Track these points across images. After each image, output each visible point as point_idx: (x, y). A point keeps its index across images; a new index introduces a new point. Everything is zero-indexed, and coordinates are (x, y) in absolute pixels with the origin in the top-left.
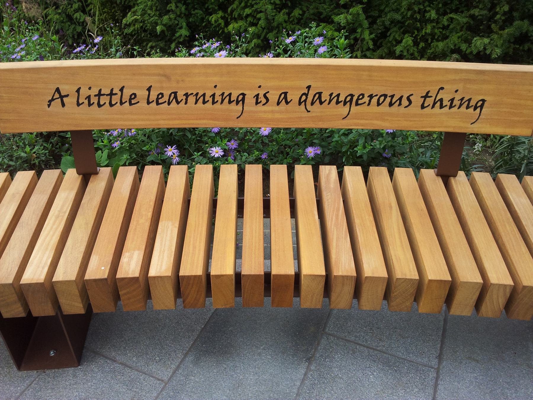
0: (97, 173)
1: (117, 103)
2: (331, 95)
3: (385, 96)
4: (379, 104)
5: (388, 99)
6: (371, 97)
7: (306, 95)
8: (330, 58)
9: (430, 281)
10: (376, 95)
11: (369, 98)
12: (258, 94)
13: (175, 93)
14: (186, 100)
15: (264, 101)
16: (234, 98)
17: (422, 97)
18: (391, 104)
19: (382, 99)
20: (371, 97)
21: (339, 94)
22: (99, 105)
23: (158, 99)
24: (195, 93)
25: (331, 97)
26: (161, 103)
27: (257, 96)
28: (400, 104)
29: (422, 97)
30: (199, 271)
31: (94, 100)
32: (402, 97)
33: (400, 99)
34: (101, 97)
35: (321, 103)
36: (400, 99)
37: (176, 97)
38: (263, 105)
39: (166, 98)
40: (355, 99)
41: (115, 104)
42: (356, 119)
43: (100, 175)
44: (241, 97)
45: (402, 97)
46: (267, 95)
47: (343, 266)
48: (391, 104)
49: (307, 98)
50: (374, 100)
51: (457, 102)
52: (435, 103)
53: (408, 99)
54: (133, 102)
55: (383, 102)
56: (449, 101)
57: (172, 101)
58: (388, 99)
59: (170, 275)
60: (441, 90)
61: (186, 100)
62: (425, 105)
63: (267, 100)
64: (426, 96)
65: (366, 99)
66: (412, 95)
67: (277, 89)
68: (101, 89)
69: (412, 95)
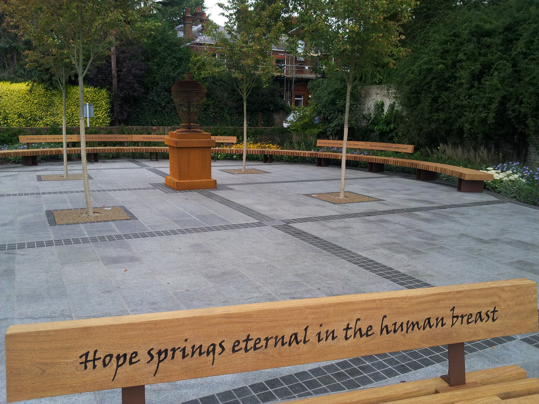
1: (262, 346)
3: (111, 356)
6: (267, 339)
10: (272, 337)
11: (265, 341)
17: (344, 330)
20: (267, 339)
23: (368, 331)
26: (370, 335)
27: (319, 334)
28: (402, 330)
31: (491, 315)
32: (402, 323)
33: (402, 325)
35: (298, 343)
36: (402, 325)
39: (473, 318)
40: (128, 357)
41: (350, 337)
42: (94, 317)
44: (212, 347)
45: (402, 323)
46: (223, 344)
51: (323, 336)
52: (355, 333)
53: (221, 345)
62: (248, 348)
64: (347, 328)
65: (263, 343)
66: (223, 341)
69: (223, 341)
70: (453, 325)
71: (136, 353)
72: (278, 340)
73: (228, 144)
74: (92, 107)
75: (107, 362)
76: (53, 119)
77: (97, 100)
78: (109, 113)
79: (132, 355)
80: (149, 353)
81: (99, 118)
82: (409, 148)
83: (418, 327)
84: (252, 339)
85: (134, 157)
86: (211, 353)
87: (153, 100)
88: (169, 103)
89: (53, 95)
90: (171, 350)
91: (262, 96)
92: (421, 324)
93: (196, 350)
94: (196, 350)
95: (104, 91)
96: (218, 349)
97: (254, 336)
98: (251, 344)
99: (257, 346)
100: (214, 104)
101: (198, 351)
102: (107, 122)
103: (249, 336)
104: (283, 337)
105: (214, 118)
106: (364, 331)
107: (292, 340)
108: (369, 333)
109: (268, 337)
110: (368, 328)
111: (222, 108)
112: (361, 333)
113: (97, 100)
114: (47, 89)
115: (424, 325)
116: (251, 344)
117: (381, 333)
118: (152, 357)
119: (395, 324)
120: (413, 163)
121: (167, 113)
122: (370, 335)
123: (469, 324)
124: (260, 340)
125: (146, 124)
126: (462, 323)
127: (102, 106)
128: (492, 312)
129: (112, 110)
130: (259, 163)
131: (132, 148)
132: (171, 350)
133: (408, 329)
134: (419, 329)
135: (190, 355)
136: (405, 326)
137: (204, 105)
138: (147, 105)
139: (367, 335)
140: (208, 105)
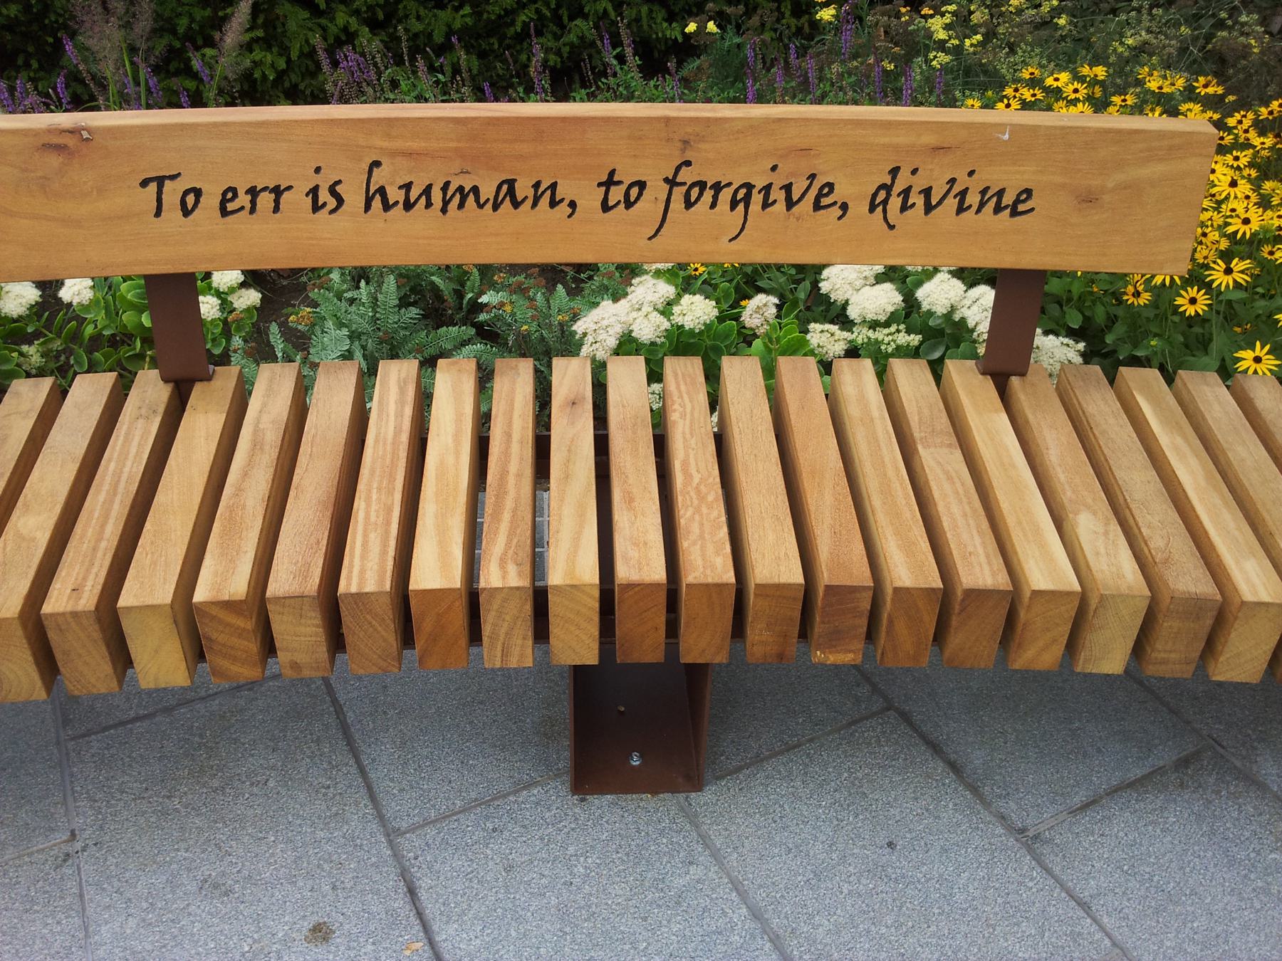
0: (208, 378)
2: (537, 185)
4: (689, 204)
6: (253, 192)
7: (888, 188)
9: (1036, 593)
10: (729, 184)
11: (249, 197)
12: (317, 187)
13: (511, 183)
15: (332, 203)
17: (600, 185)
19: (695, 193)
20: (718, 187)
21: (411, 183)
23: (1017, 201)
26: (233, 212)
27: (314, 191)
28: (429, 204)
29: (600, 185)
30: (454, 579)
32: (430, 187)
33: (427, 191)
35: (516, 204)
36: (427, 191)
37: (511, 192)
38: (332, 212)
43: (216, 383)
44: (743, 192)
45: (430, 187)
46: (338, 188)
47: (707, 562)
50: (726, 195)
51: (973, 199)
54: (230, 207)
55: (939, 203)
56: (307, 195)
59: (458, 585)
60: (684, 168)
62: (611, 203)
63: (340, 201)
64: (610, 182)
65: (244, 199)
72: (449, 194)
83: (477, 200)
84: (619, 183)
86: (741, 207)
90: (247, 192)
92: (487, 192)
93: (543, 193)
94: (543, 193)
96: (757, 198)
98: (616, 194)
103: (612, 173)
106: (1008, 199)
108: (1021, 208)
110: (224, 194)
116: (616, 194)
117: (368, 207)
119: (407, 187)
122: (233, 212)
123: (1018, 218)
124: (235, 195)
126: (713, 206)
132: (247, 192)
133: (446, 203)
134: (481, 206)
135: (975, 208)
136: (437, 196)
139: (1015, 213)
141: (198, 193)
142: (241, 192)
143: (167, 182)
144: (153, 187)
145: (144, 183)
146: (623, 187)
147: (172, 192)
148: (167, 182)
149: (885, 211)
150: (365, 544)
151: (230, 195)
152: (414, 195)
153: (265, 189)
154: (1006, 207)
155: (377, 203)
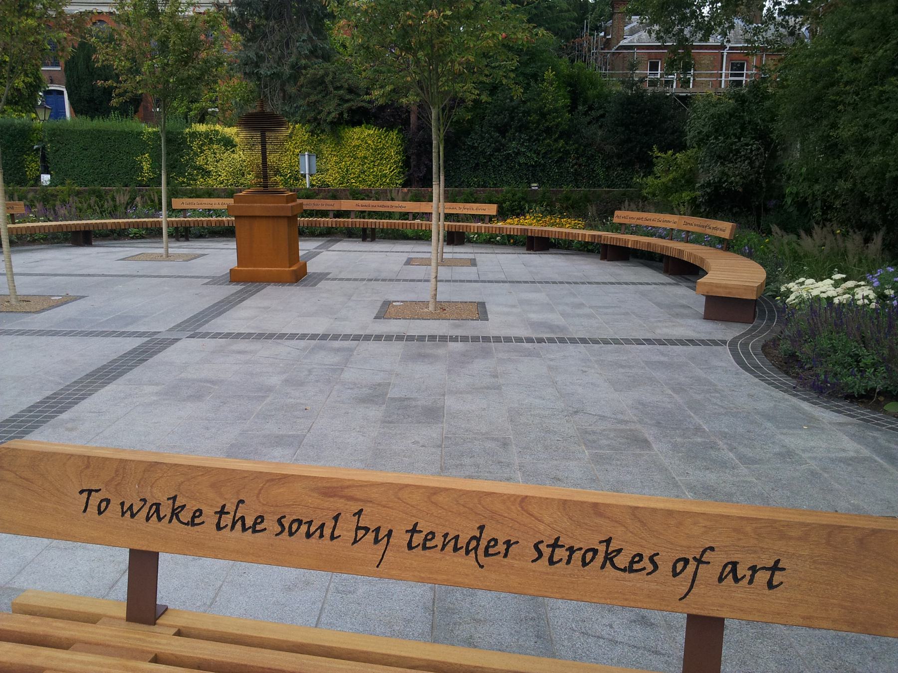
3: (300, 522)
4: (584, 564)
5: (304, 528)
7: (478, 540)
8: (527, 497)
10: (580, 549)
13: (734, 564)
14: (752, 576)
16: (462, 542)
18: (309, 535)
19: (589, 556)
22: (551, 562)
23: (255, 524)
24: (372, 528)
25: (122, 508)
29: (407, 531)
31: (547, 552)
33: (322, 526)
34: (557, 550)
35: (736, 580)
37: (734, 571)
38: (648, 574)
41: (417, 546)
48: (309, 535)
49: (478, 545)
50: (578, 555)
54: (491, 551)
57: (726, 577)
58: (304, 528)
61: (752, 576)
63: (656, 567)
64: (414, 531)
65: (501, 547)
67: (274, 513)
68: (779, 560)
70: (355, 541)
71: (262, 517)
73: (481, 218)
74: (314, 159)
75: (293, 530)
76: (320, 177)
77: (383, 148)
78: (401, 167)
79: (489, 542)
80: (536, 547)
81: (385, 176)
82: (491, 209)
85: (367, 235)
87: (473, 147)
88: (498, 150)
89: (320, 141)
91: (673, 133)
95: (393, 135)
97: (425, 527)
98: (418, 539)
99: (428, 544)
100: (577, 149)
101: (452, 543)
102: (399, 182)
104: (457, 538)
105: (576, 173)
106: (249, 522)
107: (152, 512)
108: (258, 527)
109: (510, 541)
110: (194, 513)
111: (592, 156)
112: (244, 524)
113: (383, 148)
114: (312, 133)
115: (722, 573)
116: (418, 539)
118: (540, 554)
120: (667, 247)
121: (494, 167)
125: (460, 185)
127: (389, 158)
128: (548, 546)
129: (406, 163)
130: (509, 251)
131: (329, 221)
137: (560, 152)
138: (465, 155)
140: (567, 153)
141: (108, 501)
142: (500, 543)
143: (93, 493)
144: (85, 495)
145: (81, 492)
146: (423, 535)
147: (95, 499)
148: (93, 493)
149: (476, 553)
150: (636, 230)
151: (492, 543)
152: (312, 529)
153: (763, 568)
154: (250, 528)
155: (239, 525)
